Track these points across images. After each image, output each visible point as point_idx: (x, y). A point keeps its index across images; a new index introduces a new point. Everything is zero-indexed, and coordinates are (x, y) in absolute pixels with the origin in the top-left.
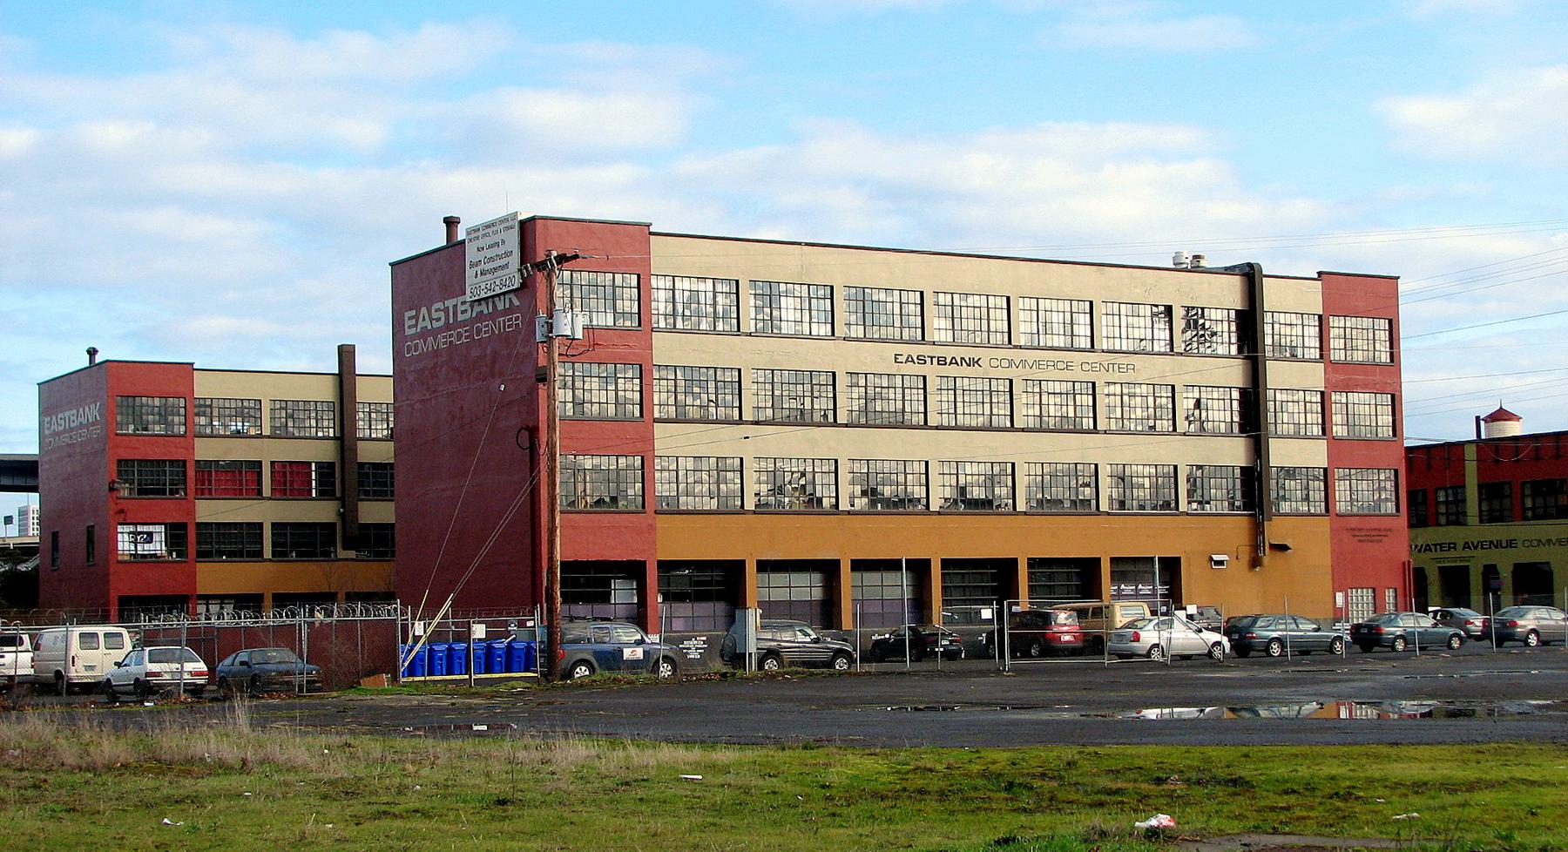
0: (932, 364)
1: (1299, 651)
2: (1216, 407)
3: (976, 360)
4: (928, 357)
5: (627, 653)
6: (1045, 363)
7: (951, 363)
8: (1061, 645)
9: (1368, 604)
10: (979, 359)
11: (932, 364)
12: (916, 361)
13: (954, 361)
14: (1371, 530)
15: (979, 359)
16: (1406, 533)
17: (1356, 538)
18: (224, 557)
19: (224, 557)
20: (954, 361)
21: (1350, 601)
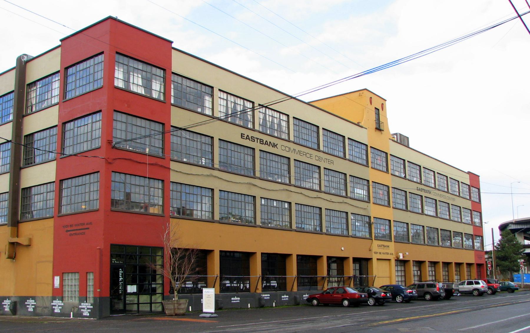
0: (257, 142)
1: (324, 304)
2: (236, 157)
3: (276, 145)
4: (256, 138)
5: (442, 295)
6: (302, 152)
7: (247, 138)
8: (362, 299)
9: (75, 291)
10: (277, 144)
11: (257, 142)
12: (250, 139)
13: (248, 138)
14: (78, 225)
15: (277, 144)
16: (393, 246)
17: (69, 233)
18: (98, 290)
19: (98, 290)
20: (266, 143)
21: (433, 272)
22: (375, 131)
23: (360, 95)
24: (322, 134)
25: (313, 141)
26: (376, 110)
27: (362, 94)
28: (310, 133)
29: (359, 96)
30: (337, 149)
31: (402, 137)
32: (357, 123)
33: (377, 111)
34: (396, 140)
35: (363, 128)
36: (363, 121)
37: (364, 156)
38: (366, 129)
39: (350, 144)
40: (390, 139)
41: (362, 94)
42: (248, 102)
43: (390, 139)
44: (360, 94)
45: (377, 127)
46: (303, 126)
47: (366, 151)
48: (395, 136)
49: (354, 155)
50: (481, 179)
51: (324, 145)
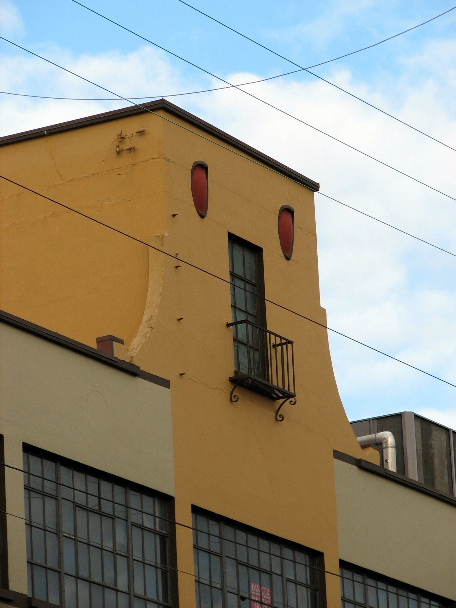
22: (233, 399)
23: (127, 145)
24: (339, 595)
25: (139, 590)
26: (238, 251)
27: (138, 142)
28: (121, 538)
29: (119, 152)
30: (122, 584)
31: (437, 440)
32: (93, 344)
33: (249, 258)
34: (392, 466)
35: (140, 382)
36: (143, 329)
37: (151, 573)
38: (165, 383)
39: (209, 552)
40: (338, 455)
41: (138, 142)
42: (90, 478)
43: (338, 455)
44: (122, 139)
45: (245, 371)
46: (205, 546)
47: (163, 538)
48: (389, 437)
49: (68, 567)
50: (333, 456)
51: (38, 559)
